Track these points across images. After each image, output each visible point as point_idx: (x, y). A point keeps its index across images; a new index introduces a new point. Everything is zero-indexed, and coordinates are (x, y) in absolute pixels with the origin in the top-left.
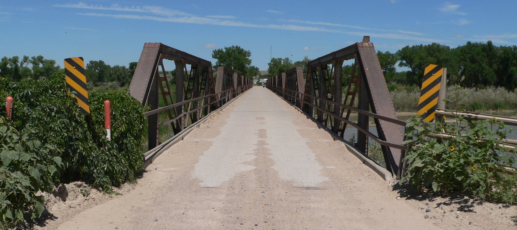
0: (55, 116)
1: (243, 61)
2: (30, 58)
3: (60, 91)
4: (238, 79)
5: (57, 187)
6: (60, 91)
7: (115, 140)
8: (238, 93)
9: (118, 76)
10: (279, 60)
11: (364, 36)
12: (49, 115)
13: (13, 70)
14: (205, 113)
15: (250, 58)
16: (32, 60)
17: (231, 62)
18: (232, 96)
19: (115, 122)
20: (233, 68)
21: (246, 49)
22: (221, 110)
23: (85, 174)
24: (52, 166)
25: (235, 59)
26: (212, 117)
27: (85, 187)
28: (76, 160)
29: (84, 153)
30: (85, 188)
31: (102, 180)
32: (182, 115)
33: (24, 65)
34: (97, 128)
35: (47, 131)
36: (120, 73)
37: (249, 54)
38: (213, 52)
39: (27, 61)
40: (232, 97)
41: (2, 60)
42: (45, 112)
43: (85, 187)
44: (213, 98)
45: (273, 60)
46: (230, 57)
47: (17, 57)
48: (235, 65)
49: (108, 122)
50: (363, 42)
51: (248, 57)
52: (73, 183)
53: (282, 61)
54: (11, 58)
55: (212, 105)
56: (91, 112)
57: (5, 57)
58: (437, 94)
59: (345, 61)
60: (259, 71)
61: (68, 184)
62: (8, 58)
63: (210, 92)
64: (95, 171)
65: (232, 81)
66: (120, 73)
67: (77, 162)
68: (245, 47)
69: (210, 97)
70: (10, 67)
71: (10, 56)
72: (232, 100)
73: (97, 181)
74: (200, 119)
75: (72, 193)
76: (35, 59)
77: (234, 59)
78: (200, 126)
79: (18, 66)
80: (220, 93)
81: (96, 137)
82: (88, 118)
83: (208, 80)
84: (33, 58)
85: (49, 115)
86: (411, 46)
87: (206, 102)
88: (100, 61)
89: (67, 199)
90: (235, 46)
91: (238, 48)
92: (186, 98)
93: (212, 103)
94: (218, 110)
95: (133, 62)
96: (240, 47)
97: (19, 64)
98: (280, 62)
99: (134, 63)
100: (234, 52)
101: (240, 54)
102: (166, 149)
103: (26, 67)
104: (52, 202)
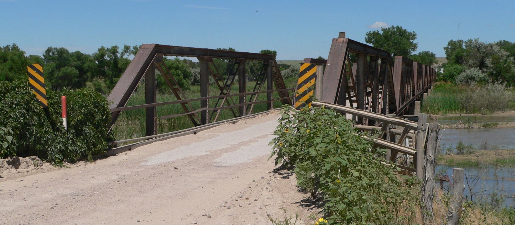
0: (15, 108)
1: (406, 46)
2: (131, 48)
3: (23, 89)
4: (418, 69)
5: (11, 158)
6: (23, 89)
9: (251, 67)
10: (459, 42)
11: (340, 32)
12: (11, 107)
13: (112, 62)
15: (415, 42)
16: (133, 50)
17: (389, 47)
19: (73, 113)
20: (393, 54)
21: (409, 30)
23: (40, 151)
24: (5, 143)
27: (38, 160)
28: (33, 141)
29: (38, 135)
30: (37, 161)
31: (54, 156)
33: (125, 57)
34: (54, 117)
35: (7, 118)
36: (254, 63)
37: (413, 36)
38: (366, 34)
39: (128, 52)
41: (99, 50)
42: (8, 104)
43: (38, 160)
45: (451, 43)
46: (388, 41)
47: (116, 47)
48: (394, 51)
50: (339, 38)
51: (411, 41)
52: (28, 157)
53: (464, 44)
54: (110, 48)
56: (48, 105)
57: (102, 47)
58: (314, 76)
59: (463, 47)
60: (436, 58)
61: (24, 157)
62: (106, 49)
64: (49, 149)
65: (412, 71)
66: (254, 63)
67: (33, 142)
68: (409, 28)
70: (108, 59)
71: (108, 46)
73: (50, 157)
75: (25, 163)
76: (137, 49)
77: (393, 43)
79: (118, 58)
81: (53, 124)
82: (46, 109)
84: (134, 48)
85: (11, 107)
88: (229, 48)
89: (20, 167)
90: (395, 26)
91: (399, 29)
95: (264, 50)
96: (401, 28)
97: (119, 55)
98: (461, 46)
99: (265, 51)
100: (394, 34)
101: (402, 37)
103: (126, 59)
104: (5, 168)
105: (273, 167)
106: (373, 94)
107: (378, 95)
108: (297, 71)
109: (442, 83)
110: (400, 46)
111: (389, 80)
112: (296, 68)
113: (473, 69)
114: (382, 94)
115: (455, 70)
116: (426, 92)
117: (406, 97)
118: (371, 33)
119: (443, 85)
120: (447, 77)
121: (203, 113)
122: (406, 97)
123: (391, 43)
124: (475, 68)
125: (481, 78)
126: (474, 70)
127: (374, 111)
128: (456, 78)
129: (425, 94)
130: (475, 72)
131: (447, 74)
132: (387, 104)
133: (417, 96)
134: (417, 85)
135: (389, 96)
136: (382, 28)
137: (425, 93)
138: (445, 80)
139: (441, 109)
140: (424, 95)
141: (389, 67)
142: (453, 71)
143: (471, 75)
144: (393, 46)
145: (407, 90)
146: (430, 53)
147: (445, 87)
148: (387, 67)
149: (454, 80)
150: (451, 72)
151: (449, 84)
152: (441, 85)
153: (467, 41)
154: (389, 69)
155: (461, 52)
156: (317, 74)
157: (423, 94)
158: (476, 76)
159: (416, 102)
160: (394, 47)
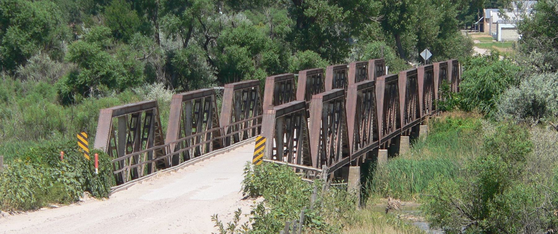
7: (100, 175)
14: (149, 171)
22: (175, 171)
26: (157, 177)
32: (124, 169)
44: (161, 152)
49: (97, 165)
55: (158, 161)
58: (264, 144)
63: (156, 142)
69: (156, 150)
72: (212, 153)
74: (141, 177)
78: (142, 183)
80: (173, 143)
83: (152, 125)
86: (144, 69)
87: (149, 157)
92: (128, 153)
93: (158, 159)
102: (118, 191)
106: (289, 154)
107: (293, 155)
111: (304, 135)
113: (542, 76)
114: (297, 154)
115: (498, 75)
117: (329, 157)
119: (455, 123)
120: (473, 97)
122: (329, 157)
131: (472, 89)
132: (341, 140)
134: (406, 111)
135: (304, 156)
138: (465, 108)
139: (417, 188)
141: (304, 118)
142: (489, 80)
145: (332, 147)
148: (302, 119)
152: (449, 123)
154: (305, 122)
156: (266, 143)
157: (378, 151)
159: (351, 167)
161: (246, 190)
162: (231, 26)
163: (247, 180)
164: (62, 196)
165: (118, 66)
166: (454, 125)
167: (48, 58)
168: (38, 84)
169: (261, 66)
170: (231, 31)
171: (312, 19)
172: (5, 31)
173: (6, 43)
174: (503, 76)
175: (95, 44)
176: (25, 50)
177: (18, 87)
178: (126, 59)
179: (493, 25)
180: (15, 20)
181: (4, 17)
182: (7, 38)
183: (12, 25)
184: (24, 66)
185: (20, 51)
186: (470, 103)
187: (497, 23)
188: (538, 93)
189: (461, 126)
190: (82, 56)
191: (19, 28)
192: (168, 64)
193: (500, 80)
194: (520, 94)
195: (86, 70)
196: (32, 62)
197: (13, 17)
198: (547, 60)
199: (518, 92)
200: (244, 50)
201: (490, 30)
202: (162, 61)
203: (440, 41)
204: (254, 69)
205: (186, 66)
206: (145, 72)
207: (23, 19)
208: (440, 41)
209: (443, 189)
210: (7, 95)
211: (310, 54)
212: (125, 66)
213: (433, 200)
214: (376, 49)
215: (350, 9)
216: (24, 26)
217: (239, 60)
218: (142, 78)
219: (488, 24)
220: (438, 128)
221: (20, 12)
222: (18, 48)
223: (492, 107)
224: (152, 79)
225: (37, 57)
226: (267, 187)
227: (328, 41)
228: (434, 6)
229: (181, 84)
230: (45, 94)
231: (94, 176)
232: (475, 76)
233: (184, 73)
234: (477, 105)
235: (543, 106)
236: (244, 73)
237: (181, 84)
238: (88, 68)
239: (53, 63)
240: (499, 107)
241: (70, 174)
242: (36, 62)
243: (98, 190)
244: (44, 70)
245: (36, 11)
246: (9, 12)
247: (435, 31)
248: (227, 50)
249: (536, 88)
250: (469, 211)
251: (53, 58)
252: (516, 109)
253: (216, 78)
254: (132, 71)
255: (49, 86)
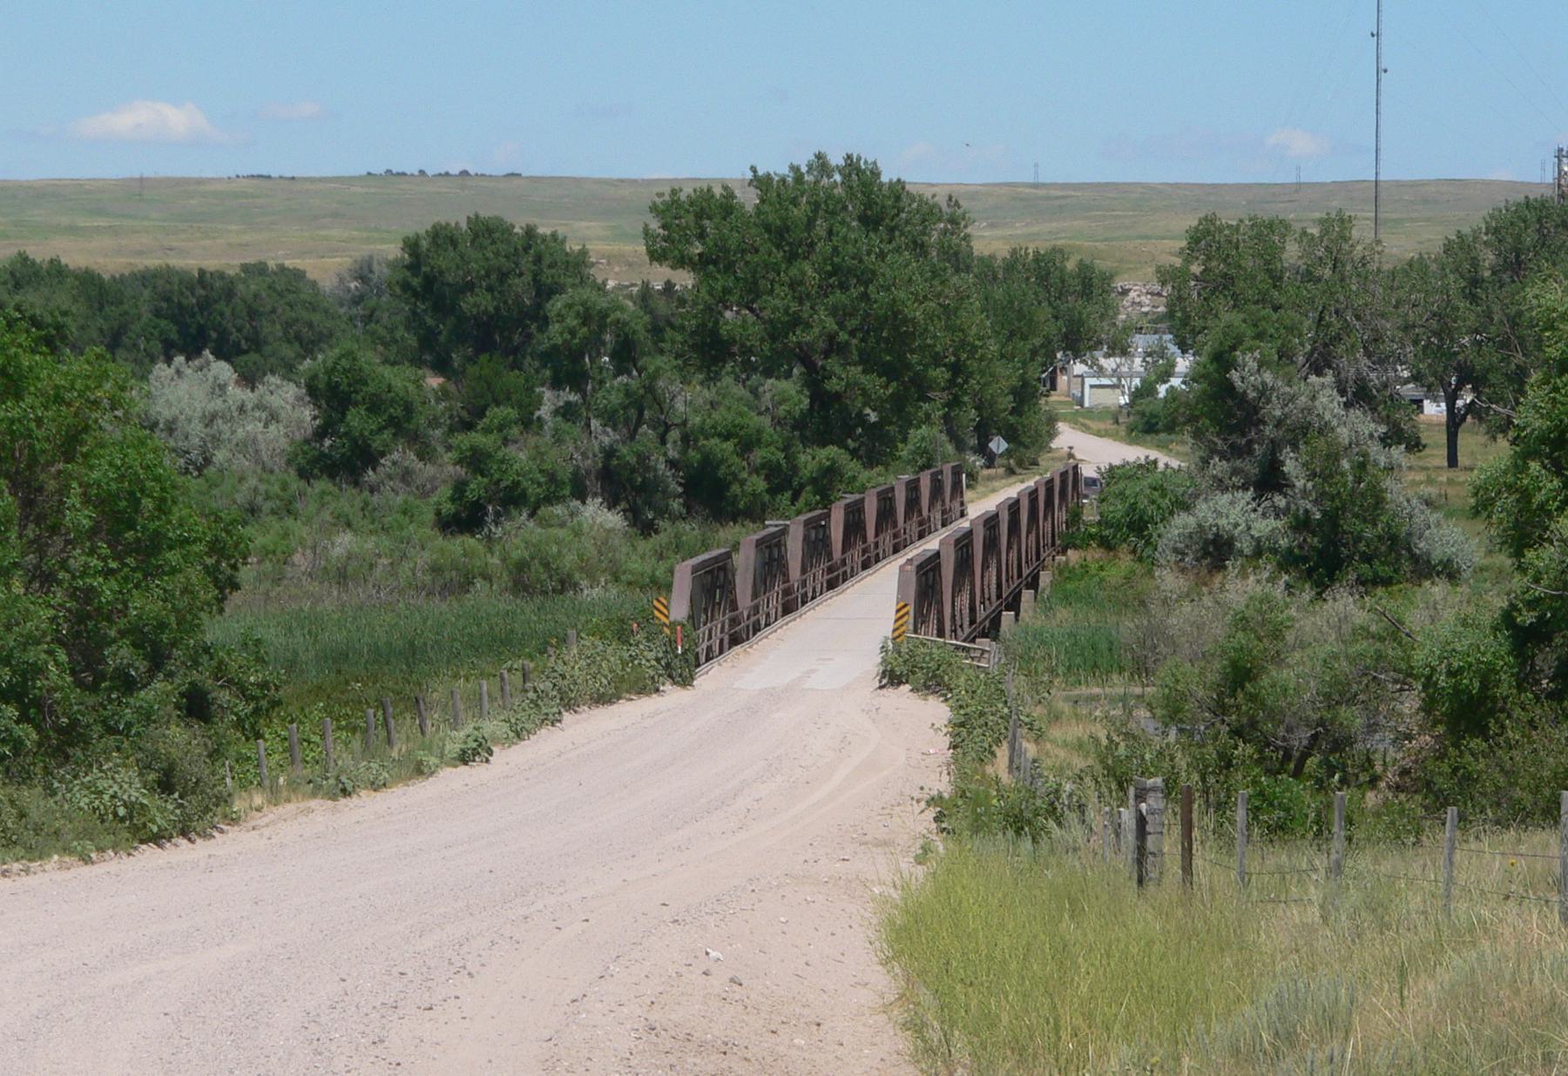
8: (845, 572)
18: (780, 609)
25: (838, 274)
40: (780, 613)
46: (792, 258)
58: (907, 613)
90: (836, 159)
91: (860, 176)
94: (746, 645)
96: (876, 174)
105: (878, 685)
108: (170, 429)
109: (1095, 554)
110: (865, 296)
112: (167, 414)
113: (1227, 497)
116: (1014, 604)
118: (683, 197)
119: (1093, 567)
121: (709, 649)
123: (810, 272)
124: (1240, 494)
125: (1258, 540)
126: (1232, 503)
127: (956, 639)
128: (1155, 535)
129: (1008, 616)
130: (1235, 514)
131: (1118, 515)
133: (981, 623)
136: (754, 169)
137: (1007, 610)
138: (1106, 544)
140: (1003, 618)
142: (1143, 503)
143: (1217, 525)
144: (824, 291)
146: (1070, 265)
147: (1102, 580)
149: (1148, 543)
150: (1133, 507)
151: (1125, 561)
153: (1314, 231)
155: (1250, 332)
158: (1236, 532)
160: (831, 300)
161: (883, 677)
162: (708, 407)
163: (884, 661)
164: (640, 685)
165: (530, 471)
166: (1093, 571)
167: (413, 457)
168: (400, 499)
169: (756, 471)
170: (710, 416)
171: (837, 396)
172: (344, 415)
173: (346, 434)
174: (1164, 496)
175: (492, 437)
176: (376, 444)
177: (366, 504)
178: (543, 460)
179: (1075, 380)
180: (359, 398)
181: (343, 392)
182: (348, 425)
183: (356, 404)
184: (374, 470)
185: (370, 446)
186: (1114, 537)
187: (1082, 377)
188: (1223, 522)
189: (1103, 573)
190: (473, 455)
191: (367, 409)
192: (606, 468)
193: (1160, 500)
194: (1194, 525)
195: (480, 478)
196: (388, 463)
197: (356, 392)
198: (1235, 472)
199: (1191, 520)
200: (729, 446)
201: (1069, 386)
202: (595, 463)
203: (1012, 419)
204: (746, 476)
205: (633, 470)
206: (571, 481)
207: (374, 395)
208: (1012, 419)
209: (1180, 677)
210: (351, 517)
211: (832, 450)
212: (541, 471)
213: (1167, 691)
214: (923, 439)
215: (896, 379)
216: (375, 406)
217: (723, 461)
218: (567, 492)
219: (1065, 378)
220: (1067, 574)
221: (366, 384)
222: (364, 441)
223: (1148, 543)
224: (581, 494)
225: (395, 456)
226: (914, 673)
227: (860, 430)
228: (1004, 361)
229: (626, 498)
230: (412, 516)
231: (676, 656)
232: (1121, 495)
233: (630, 480)
234: (1125, 540)
235: (1230, 543)
236: (730, 483)
237: (626, 498)
238: (483, 475)
239: (421, 465)
240: (1161, 544)
241: (651, 655)
242: (394, 463)
243: (681, 676)
244: (406, 476)
245: (393, 383)
246: (350, 385)
247: (1007, 402)
248: (703, 446)
249: (1219, 514)
250: (1212, 705)
251: (421, 457)
252: (1187, 546)
253: (680, 490)
254: (552, 477)
255: (418, 502)
